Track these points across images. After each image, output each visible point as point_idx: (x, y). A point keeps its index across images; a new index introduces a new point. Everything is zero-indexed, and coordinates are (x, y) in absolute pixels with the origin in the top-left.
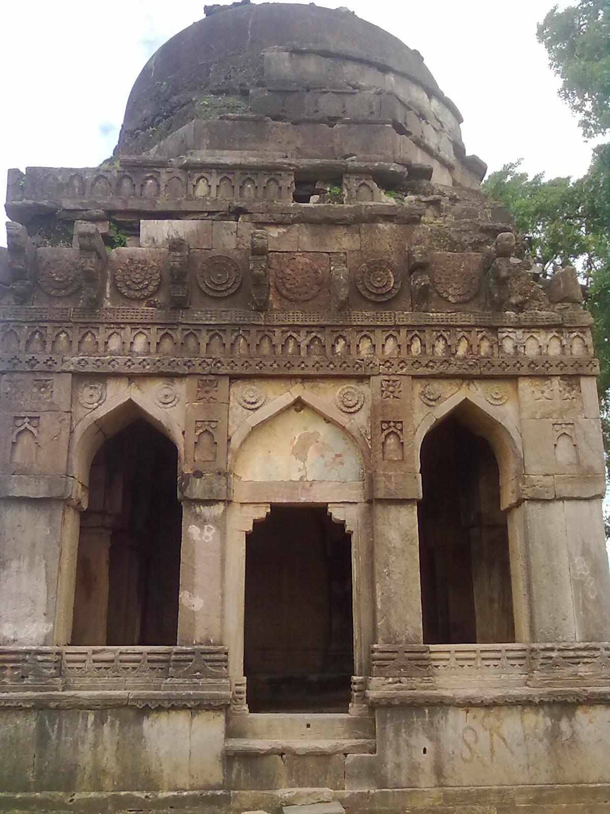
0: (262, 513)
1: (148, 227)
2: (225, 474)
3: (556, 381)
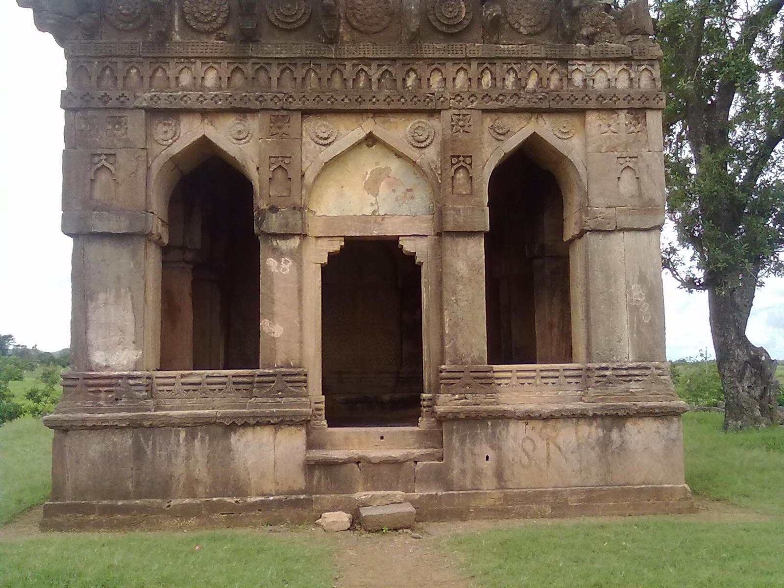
0: (336, 246)
2: (299, 209)
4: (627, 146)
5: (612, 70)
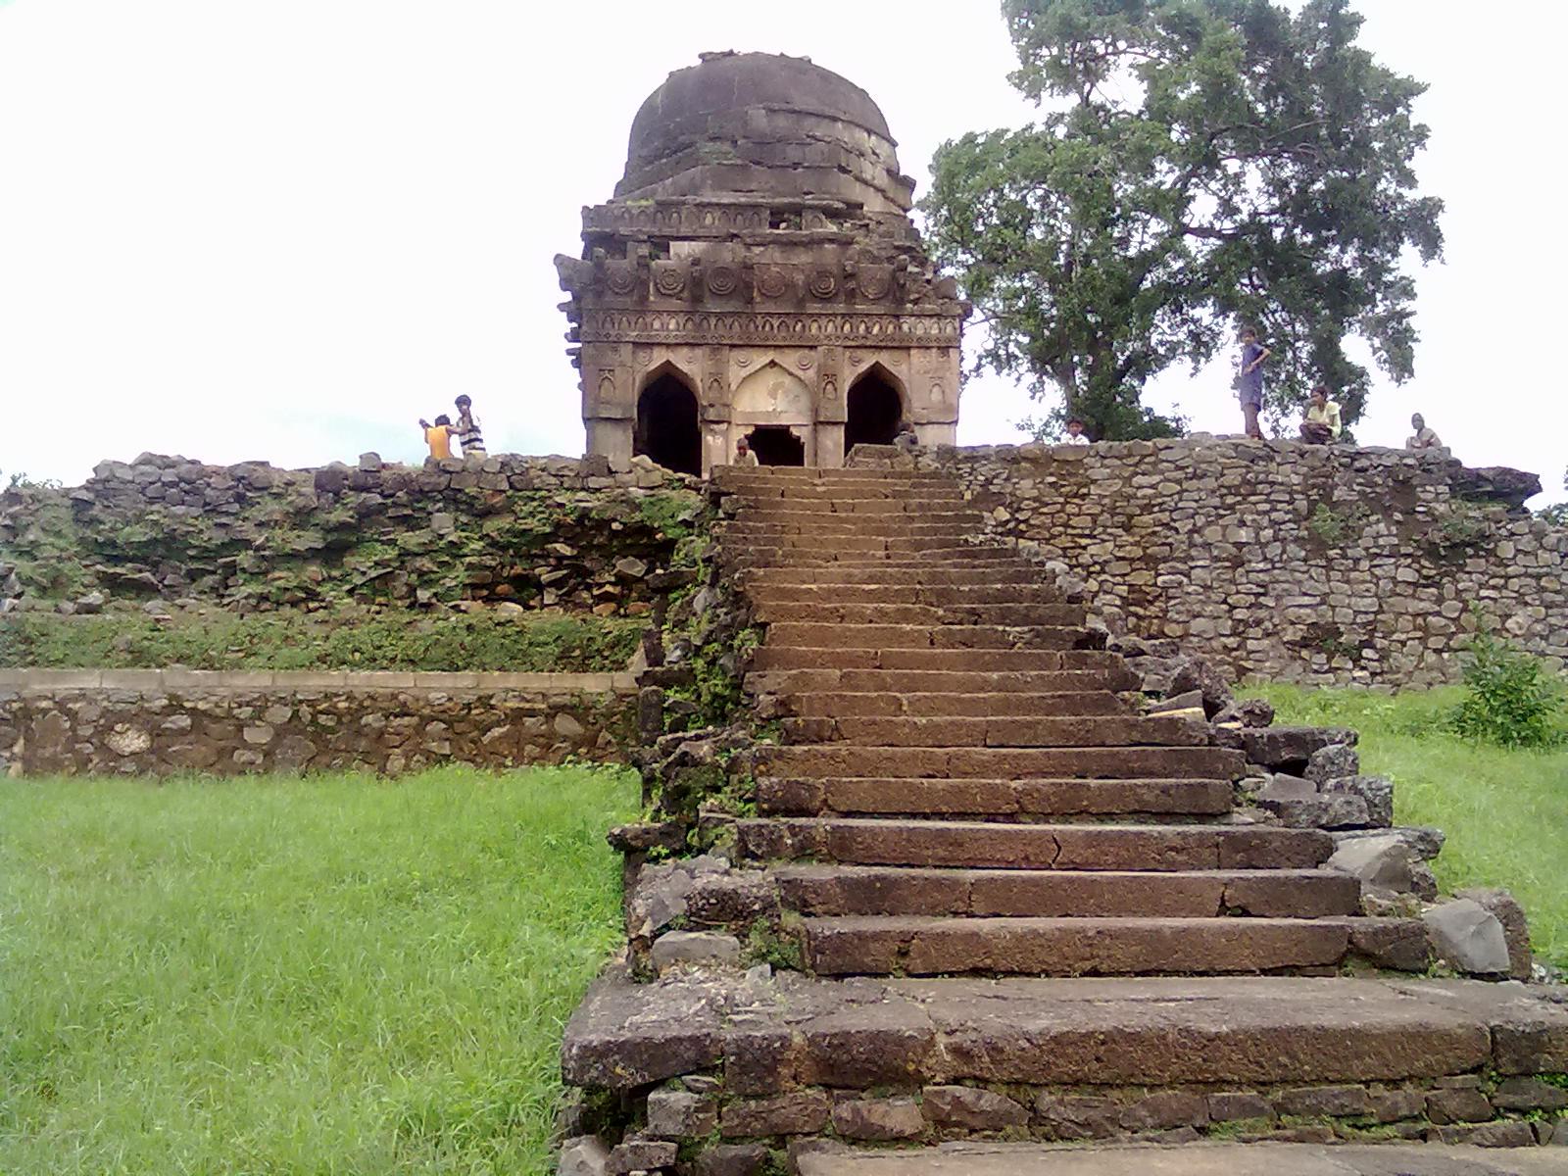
0: (750, 431)
1: (675, 247)
4: (936, 370)
5: (927, 322)
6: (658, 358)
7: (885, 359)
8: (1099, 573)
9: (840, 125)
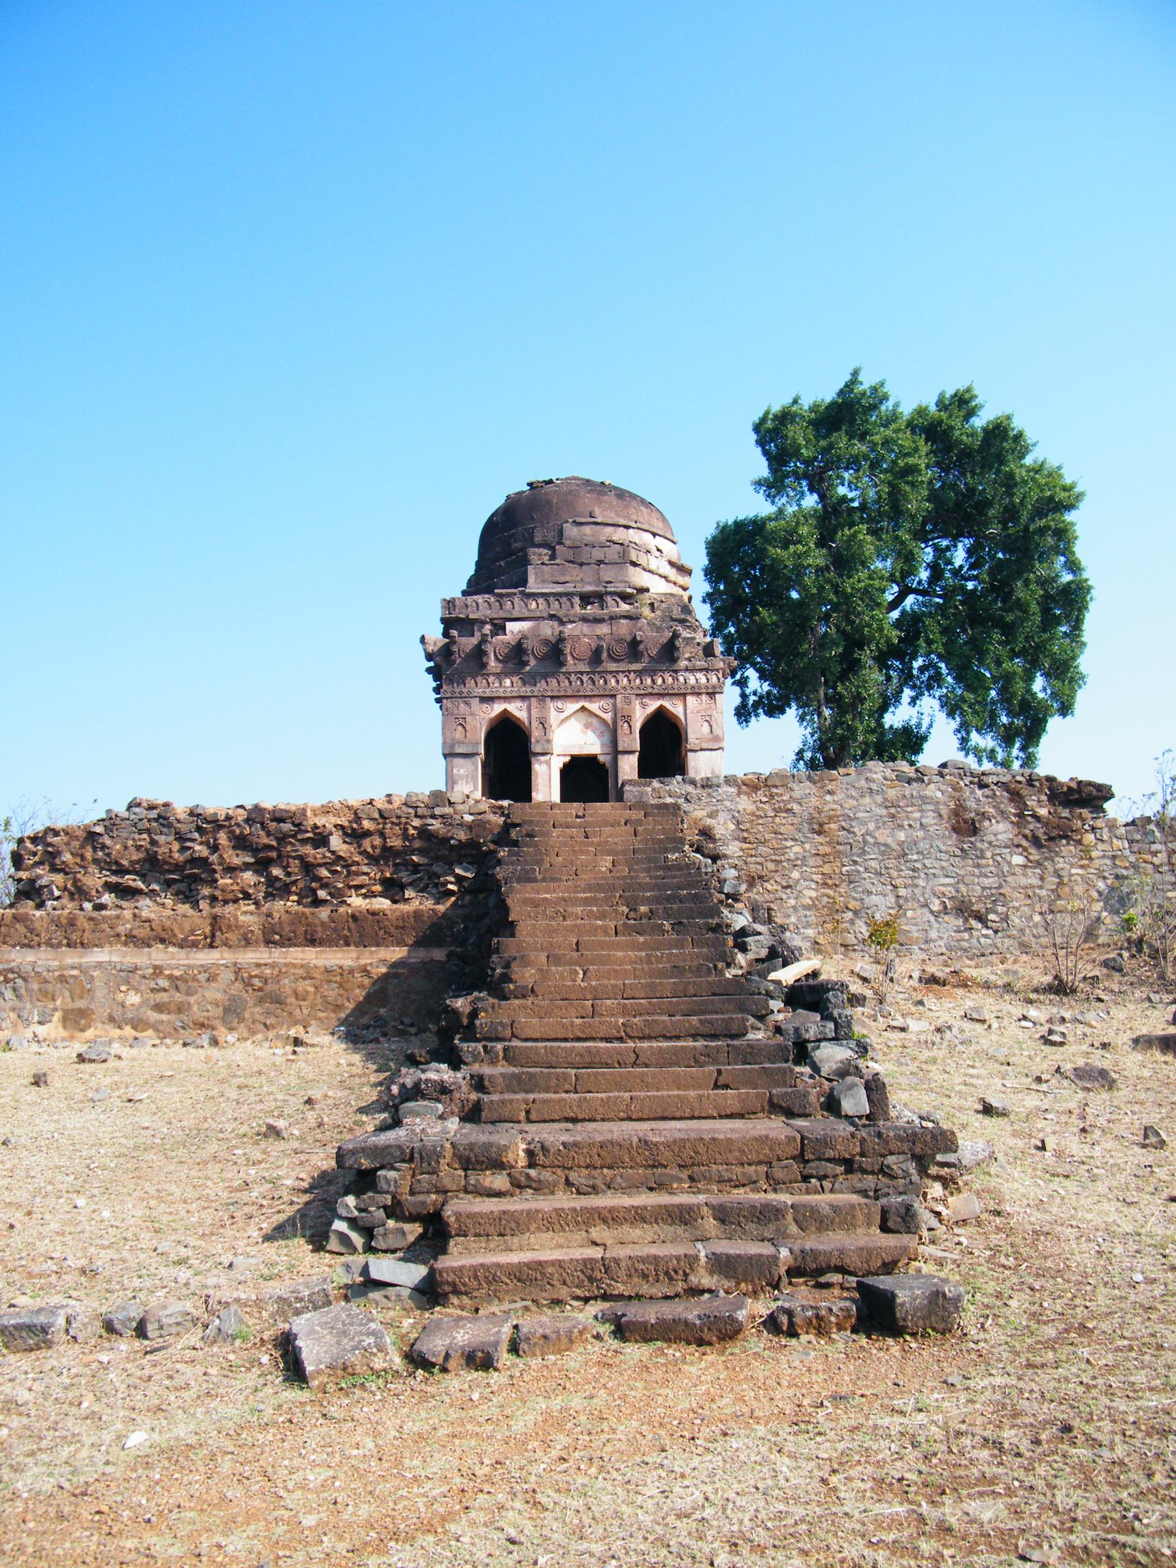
0: (567, 759)
1: (511, 626)
2: (549, 741)
3: (704, 697)
4: (706, 710)
5: (699, 675)
6: (498, 708)
7: (667, 703)
8: (801, 867)
9: (631, 531)
